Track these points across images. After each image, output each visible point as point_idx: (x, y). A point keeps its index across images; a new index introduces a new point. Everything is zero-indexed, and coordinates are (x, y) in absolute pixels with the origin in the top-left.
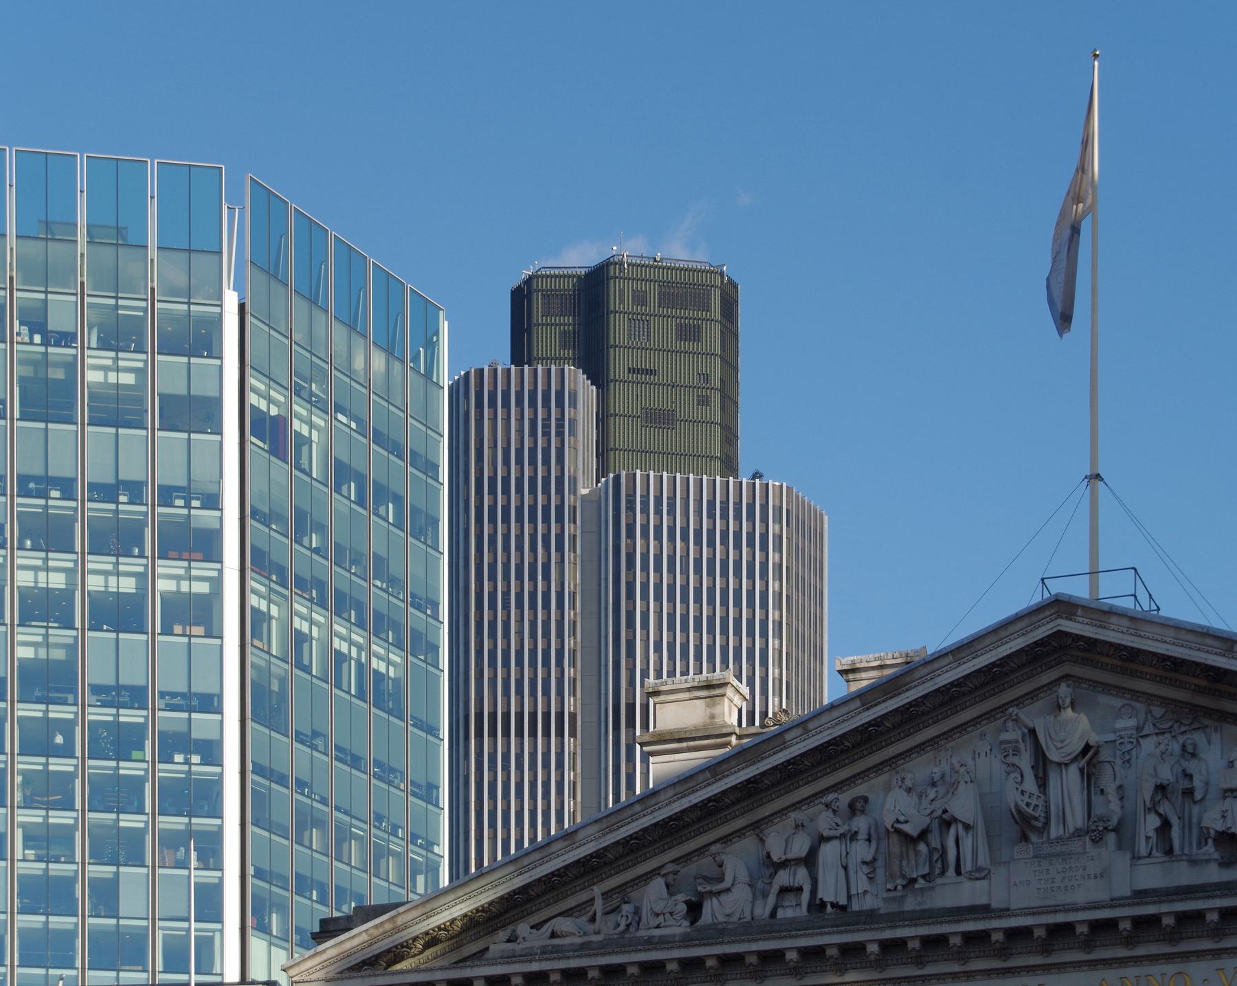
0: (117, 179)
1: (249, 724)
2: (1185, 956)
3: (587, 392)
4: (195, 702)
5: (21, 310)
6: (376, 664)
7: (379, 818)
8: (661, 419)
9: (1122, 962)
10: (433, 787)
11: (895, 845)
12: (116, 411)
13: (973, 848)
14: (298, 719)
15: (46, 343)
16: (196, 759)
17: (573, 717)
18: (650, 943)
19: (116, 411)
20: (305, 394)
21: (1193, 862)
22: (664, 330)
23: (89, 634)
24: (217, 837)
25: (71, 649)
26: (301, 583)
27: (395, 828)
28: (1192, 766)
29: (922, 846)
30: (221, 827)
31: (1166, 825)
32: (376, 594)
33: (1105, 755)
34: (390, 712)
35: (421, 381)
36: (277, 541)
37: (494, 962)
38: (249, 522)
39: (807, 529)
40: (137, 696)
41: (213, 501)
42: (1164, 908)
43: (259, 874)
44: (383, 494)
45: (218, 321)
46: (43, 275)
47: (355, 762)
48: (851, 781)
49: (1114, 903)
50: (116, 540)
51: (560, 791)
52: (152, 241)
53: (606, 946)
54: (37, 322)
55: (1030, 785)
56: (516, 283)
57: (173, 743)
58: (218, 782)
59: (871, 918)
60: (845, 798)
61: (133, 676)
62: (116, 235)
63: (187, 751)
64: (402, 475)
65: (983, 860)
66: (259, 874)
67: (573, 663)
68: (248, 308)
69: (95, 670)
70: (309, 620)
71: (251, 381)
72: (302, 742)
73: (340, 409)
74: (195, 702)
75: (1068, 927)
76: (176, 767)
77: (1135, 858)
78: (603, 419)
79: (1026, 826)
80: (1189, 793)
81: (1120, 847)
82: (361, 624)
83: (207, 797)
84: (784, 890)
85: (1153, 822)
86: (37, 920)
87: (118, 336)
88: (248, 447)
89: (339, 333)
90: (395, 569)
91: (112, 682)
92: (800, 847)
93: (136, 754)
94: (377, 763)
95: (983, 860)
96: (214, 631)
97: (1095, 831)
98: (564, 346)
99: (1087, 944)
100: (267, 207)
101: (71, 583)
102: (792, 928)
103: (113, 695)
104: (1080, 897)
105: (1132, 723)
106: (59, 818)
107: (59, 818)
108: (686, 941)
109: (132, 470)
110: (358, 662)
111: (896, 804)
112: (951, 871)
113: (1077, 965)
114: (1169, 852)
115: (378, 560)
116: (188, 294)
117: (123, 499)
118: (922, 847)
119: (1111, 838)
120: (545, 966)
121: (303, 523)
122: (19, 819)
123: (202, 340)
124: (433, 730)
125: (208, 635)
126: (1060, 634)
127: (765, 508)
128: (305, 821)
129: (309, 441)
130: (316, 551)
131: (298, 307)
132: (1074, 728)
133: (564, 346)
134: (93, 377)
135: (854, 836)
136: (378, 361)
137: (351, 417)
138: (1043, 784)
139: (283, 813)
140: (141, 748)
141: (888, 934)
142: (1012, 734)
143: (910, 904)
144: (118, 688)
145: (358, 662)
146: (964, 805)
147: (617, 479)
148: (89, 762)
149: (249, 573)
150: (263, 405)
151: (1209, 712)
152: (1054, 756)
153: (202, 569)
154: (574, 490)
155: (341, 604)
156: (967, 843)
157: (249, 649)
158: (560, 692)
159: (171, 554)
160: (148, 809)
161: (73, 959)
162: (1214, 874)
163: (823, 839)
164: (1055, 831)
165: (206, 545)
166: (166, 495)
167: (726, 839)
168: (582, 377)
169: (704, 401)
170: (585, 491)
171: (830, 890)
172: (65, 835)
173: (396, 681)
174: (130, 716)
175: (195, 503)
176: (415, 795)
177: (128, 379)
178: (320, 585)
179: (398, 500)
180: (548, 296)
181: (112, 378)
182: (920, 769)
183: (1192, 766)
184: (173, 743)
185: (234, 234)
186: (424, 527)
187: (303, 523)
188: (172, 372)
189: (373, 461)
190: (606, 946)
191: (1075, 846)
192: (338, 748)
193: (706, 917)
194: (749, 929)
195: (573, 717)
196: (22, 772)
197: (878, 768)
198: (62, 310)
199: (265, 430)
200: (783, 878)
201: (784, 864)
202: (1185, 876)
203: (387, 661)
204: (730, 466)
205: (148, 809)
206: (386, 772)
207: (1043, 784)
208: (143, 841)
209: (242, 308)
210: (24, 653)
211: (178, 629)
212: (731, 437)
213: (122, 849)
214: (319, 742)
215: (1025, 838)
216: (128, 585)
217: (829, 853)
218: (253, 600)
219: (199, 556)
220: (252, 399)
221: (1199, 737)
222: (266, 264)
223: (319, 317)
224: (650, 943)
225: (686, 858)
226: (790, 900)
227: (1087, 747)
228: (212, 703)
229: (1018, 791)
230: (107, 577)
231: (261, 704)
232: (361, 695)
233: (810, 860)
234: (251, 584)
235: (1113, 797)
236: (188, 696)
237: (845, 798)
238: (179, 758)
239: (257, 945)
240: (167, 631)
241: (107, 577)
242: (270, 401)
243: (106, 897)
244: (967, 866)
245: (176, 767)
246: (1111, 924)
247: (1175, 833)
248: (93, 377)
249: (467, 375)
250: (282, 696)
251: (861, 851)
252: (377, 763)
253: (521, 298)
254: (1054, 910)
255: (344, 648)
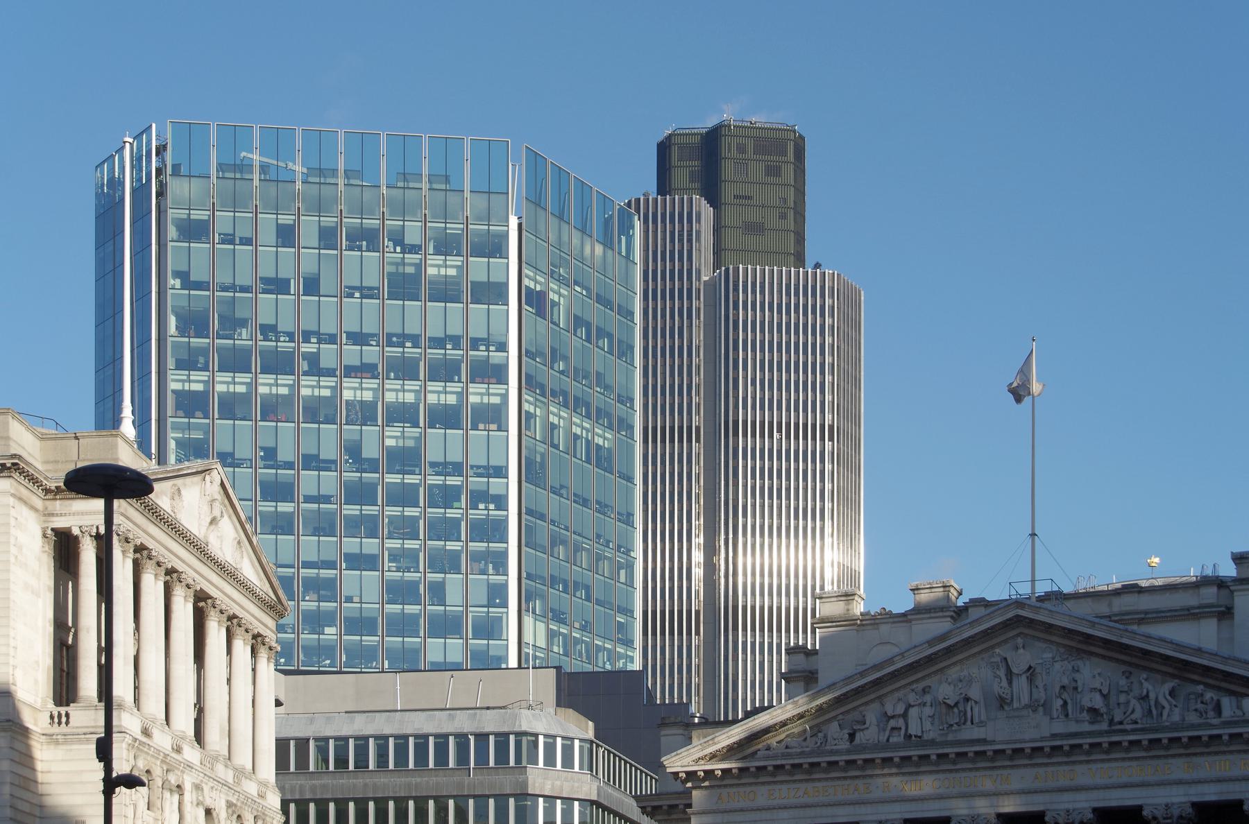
0: (447, 148)
1: (524, 483)
2: (1074, 763)
3: (707, 211)
4: (491, 471)
5: (389, 231)
6: (600, 441)
7: (599, 536)
8: (755, 228)
9: (1046, 765)
10: (630, 515)
11: (944, 710)
12: (445, 292)
13: (979, 712)
14: (552, 479)
15: (403, 252)
16: (492, 506)
17: (698, 429)
18: (832, 752)
19: (445, 292)
20: (556, 276)
21: (1077, 721)
22: (757, 170)
23: (429, 430)
24: (504, 554)
25: (418, 439)
26: (554, 394)
27: (608, 542)
28: (1077, 676)
29: (957, 710)
30: (507, 549)
31: (1065, 703)
32: (596, 396)
33: (1038, 670)
34: (605, 470)
35: (624, 261)
36: (537, 366)
37: (760, 759)
38: (524, 358)
39: (849, 300)
40: (457, 469)
41: (503, 347)
42: (1065, 742)
43: (529, 577)
44: (602, 333)
45: (506, 236)
46: (402, 210)
47: (585, 503)
48: (923, 678)
49: (1042, 739)
50: (445, 372)
51: (689, 479)
52: (467, 187)
53: (811, 754)
54: (398, 239)
55: (1005, 683)
56: (661, 138)
57: (479, 497)
58: (506, 520)
59: (932, 743)
60: (921, 685)
61: (455, 456)
62: (444, 179)
63: (487, 502)
64: (613, 320)
65: (983, 718)
66: (529, 577)
67: (698, 393)
68: (524, 226)
69: (433, 453)
70: (558, 415)
71: (526, 271)
72: (554, 493)
73: (576, 283)
74: (491, 471)
75: (1022, 750)
76: (480, 512)
77: (1052, 719)
78: (718, 230)
79: (1002, 702)
80: (1076, 688)
81: (1045, 714)
82: (588, 416)
83: (497, 530)
84: (893, 729)
85: (1060, 702)
86: (397, 608)
87: (446, 246)
88: (524, 312)
89: (576, 238)
90: (608, 380)
91: (442, 460)
92: (900, 709)
93: (456, 504)
94: (598, 502)
95: (983, 718)
96: (503, 427)
97: (1033, 706)
98: (691, 181)
99: (1030, 757)
100: (535, 161)
101: (418, 399)
102: (897, 747)
103: (444, 468)
104: (1027, 737)
105: (1050, 655)
106: (411, 544)
107: (411, 544)
108: (848, 752)
109: (455, 329)
110: (587, 440)
111: (946, 691)
112: (969, 722)
113: (1025, 766)
114: (1067, 715)
115: (598, 374)
116: (487, 218)
117: (449, 346)
118: (956, 710)
119: (1041, 709)
120: (783, 762)
121: (556, 355)
122: (386, 545)
123: (496, 248)
124: (630, 479)
125: (499, 430)
126: (1017, 616)
127: (823, 288)
128: (556, 541)
129: (559, 304)
130: (562, 372)
131: (553, 222)
132: (1022, 659)
133: (691, 181)
134: (431, 271)
135: (925, 704)
136: (599, 249)
137: (583, 287)
138: (1010, 683)
139: (543, 538)
140: (459, 500)
141: (940, 751)
142: (997, 659)
143: (950, 737)
144: (445, 464)
145: (587, 440)
146: (975, 693)
147: (727, 270)
148: (429, 510)
149: (524, 390)
150: (532, 285)
151: (1085, 652)
152: (1015, 670)
153: (496, 389)
154: (699, 278)
155: (577, 404)
156: (976, 710)
157: (524, 437)
158: (690, 413)
159: (477, 380)
160: (463, 538)
161: (418, 631)
162: (1086, 727)
163: (910, 706)
164: (1016, 705)
165: (499, 374)
166: (475, 343)
167: (866, 703)
168: (704, 202)
169: (783, 216)
170: (707, 278)
171: (914, 730)
172: (413, 555)
173: (609, 450)
174: (453, 481)
175: (492, 348)
176: (620, 520)
177: (452, 272)
178: (564, 393)
179: (610, 336)
180: (682, 147)
181: (443, 271)
182: (954, 673)
183: (1077, 676)
184: (479, 497)
185: (516, 180)
186: (625, 351)
187: (556, 355)
188: (479, 268)
189: (595, 313)
190: (811, 754)
191: (1024, 712)
192: (575, 495)
193: (857, 740)
194: (877, 747)
195: (698, 429)
196: (389, 517)
197: (935, 673)
198: (413, 232)
199: (534, 300)
200: (892, 723)
201: (893, 717)
202: (1073, 728)
203: (603, 438)
204: (800, 260)
205: (463, 538)
206: (603, 508)
207: (1010, 683)
208: (460, 557)
209: (520, 225)
210: (390, 442)
211: (481, 426)
212: (800, 239)
213: (449, 563)
214: (564, 492)
215: (1002, 707)
216: (452, 400)
217: (913, 712)
218: (526, 406)
219: (494, 380)
220: (526, 282)
221: (1079, 663)
222: (535, 200)
223: (565, 227)
224: (832, 752)
225: (848, 712)
226: (896, 733)
227: (1030, 667)
228: (501, 472)
229: (1000, 686)
230: (440, 394)
231: (531, 471)
232: (588, 461)
233: (905, 715)
234: (525, 397)
235: (1041, 690)
236: (487, 468)
237: (921, 685)
238: (481, 506)
239: (528, 621)
240: (475, 428)
241: (440, 394)
242: (536, 282)
243: (438, 592)
244: (976, 720)
245: (480, 512)
246: (1041, 749)
247: (1070, 707)
248: (431, 271)
249: (630, 202)
250: (543, 465)
251: (928, 711)
252: (598, 502)
253: (664, 148)
254: (1015, 742)
255: (578, 431)
